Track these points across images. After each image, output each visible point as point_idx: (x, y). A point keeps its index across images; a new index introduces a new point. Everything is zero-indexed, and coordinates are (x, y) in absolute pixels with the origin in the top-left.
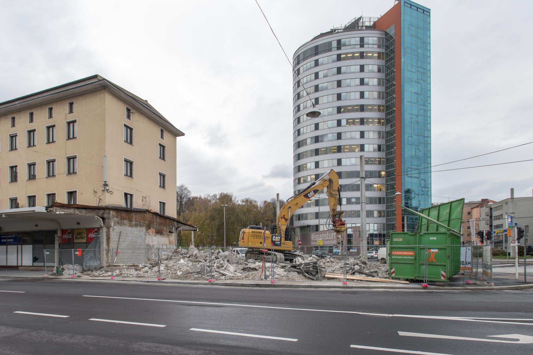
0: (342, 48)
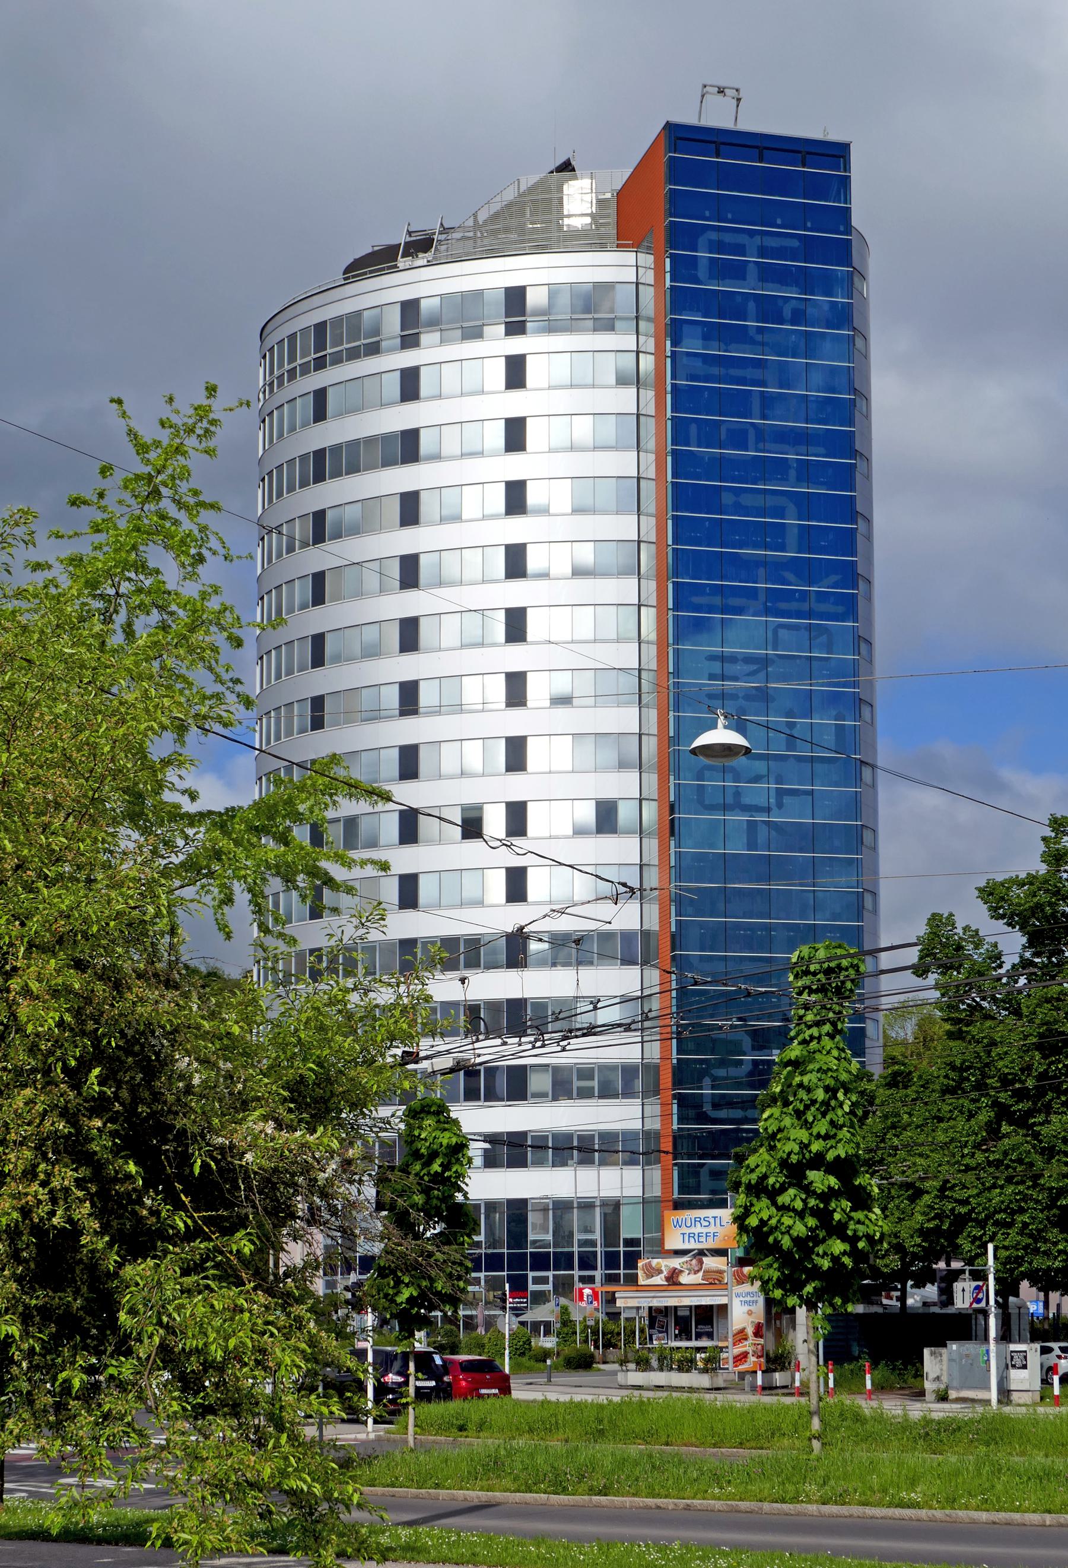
0: (424, 339)
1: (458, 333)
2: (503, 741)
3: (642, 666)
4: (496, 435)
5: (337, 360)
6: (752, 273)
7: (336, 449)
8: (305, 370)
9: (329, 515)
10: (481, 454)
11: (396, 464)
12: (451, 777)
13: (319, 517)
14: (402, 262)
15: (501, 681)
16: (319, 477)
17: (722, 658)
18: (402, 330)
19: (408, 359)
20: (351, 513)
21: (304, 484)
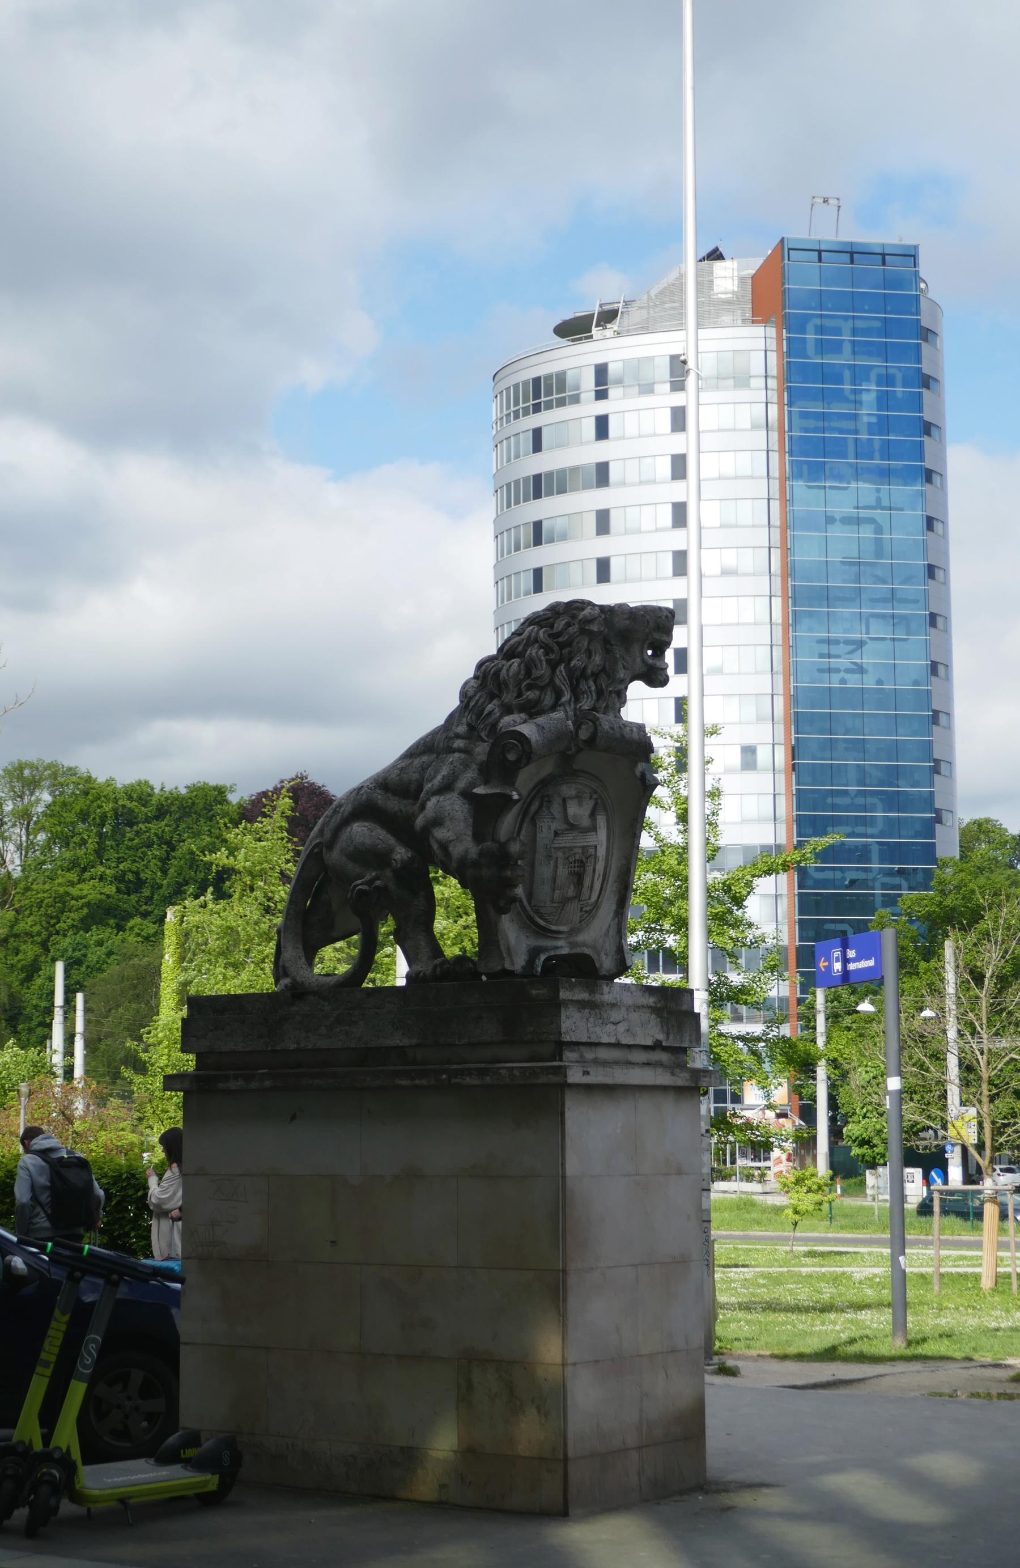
0: (612, 393)
1: (636, 389)
2: (671, 553)
3: (771, 496)
4: (665, 467)
5: (549, 406)
6: (847, 348)
7: (550, 475)
8: (526, 412)
9: (545, 525)
10: (654, 482)
11: (592, 488)
12: (633, 485)
13: (538, 526)
14: (595, 331)
15: (669, 508)
16: (537, 495)
17: (829, 642)
18: (597, 386)
19: (601, 408)
20: (560, 524)
21: (526, 499)
